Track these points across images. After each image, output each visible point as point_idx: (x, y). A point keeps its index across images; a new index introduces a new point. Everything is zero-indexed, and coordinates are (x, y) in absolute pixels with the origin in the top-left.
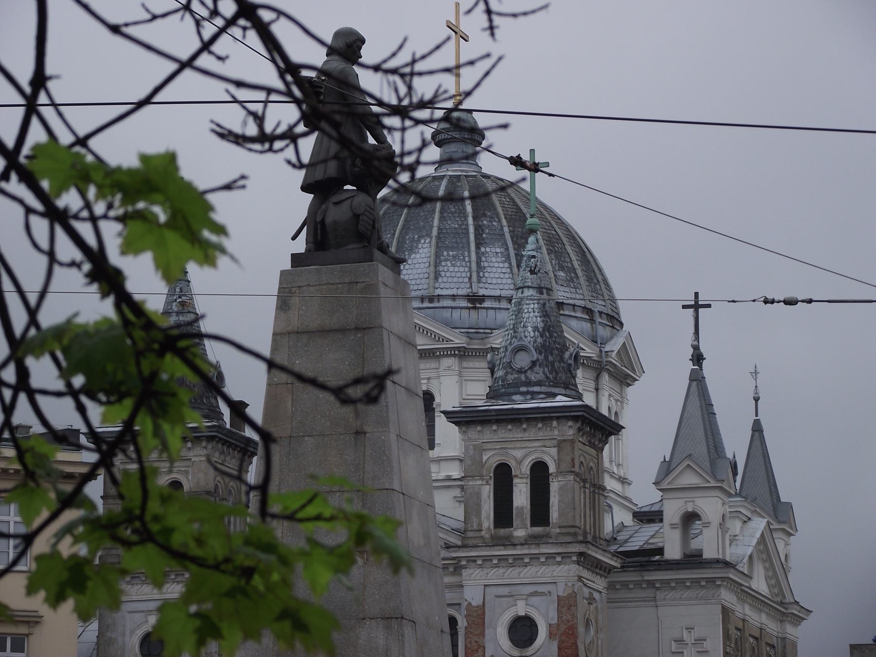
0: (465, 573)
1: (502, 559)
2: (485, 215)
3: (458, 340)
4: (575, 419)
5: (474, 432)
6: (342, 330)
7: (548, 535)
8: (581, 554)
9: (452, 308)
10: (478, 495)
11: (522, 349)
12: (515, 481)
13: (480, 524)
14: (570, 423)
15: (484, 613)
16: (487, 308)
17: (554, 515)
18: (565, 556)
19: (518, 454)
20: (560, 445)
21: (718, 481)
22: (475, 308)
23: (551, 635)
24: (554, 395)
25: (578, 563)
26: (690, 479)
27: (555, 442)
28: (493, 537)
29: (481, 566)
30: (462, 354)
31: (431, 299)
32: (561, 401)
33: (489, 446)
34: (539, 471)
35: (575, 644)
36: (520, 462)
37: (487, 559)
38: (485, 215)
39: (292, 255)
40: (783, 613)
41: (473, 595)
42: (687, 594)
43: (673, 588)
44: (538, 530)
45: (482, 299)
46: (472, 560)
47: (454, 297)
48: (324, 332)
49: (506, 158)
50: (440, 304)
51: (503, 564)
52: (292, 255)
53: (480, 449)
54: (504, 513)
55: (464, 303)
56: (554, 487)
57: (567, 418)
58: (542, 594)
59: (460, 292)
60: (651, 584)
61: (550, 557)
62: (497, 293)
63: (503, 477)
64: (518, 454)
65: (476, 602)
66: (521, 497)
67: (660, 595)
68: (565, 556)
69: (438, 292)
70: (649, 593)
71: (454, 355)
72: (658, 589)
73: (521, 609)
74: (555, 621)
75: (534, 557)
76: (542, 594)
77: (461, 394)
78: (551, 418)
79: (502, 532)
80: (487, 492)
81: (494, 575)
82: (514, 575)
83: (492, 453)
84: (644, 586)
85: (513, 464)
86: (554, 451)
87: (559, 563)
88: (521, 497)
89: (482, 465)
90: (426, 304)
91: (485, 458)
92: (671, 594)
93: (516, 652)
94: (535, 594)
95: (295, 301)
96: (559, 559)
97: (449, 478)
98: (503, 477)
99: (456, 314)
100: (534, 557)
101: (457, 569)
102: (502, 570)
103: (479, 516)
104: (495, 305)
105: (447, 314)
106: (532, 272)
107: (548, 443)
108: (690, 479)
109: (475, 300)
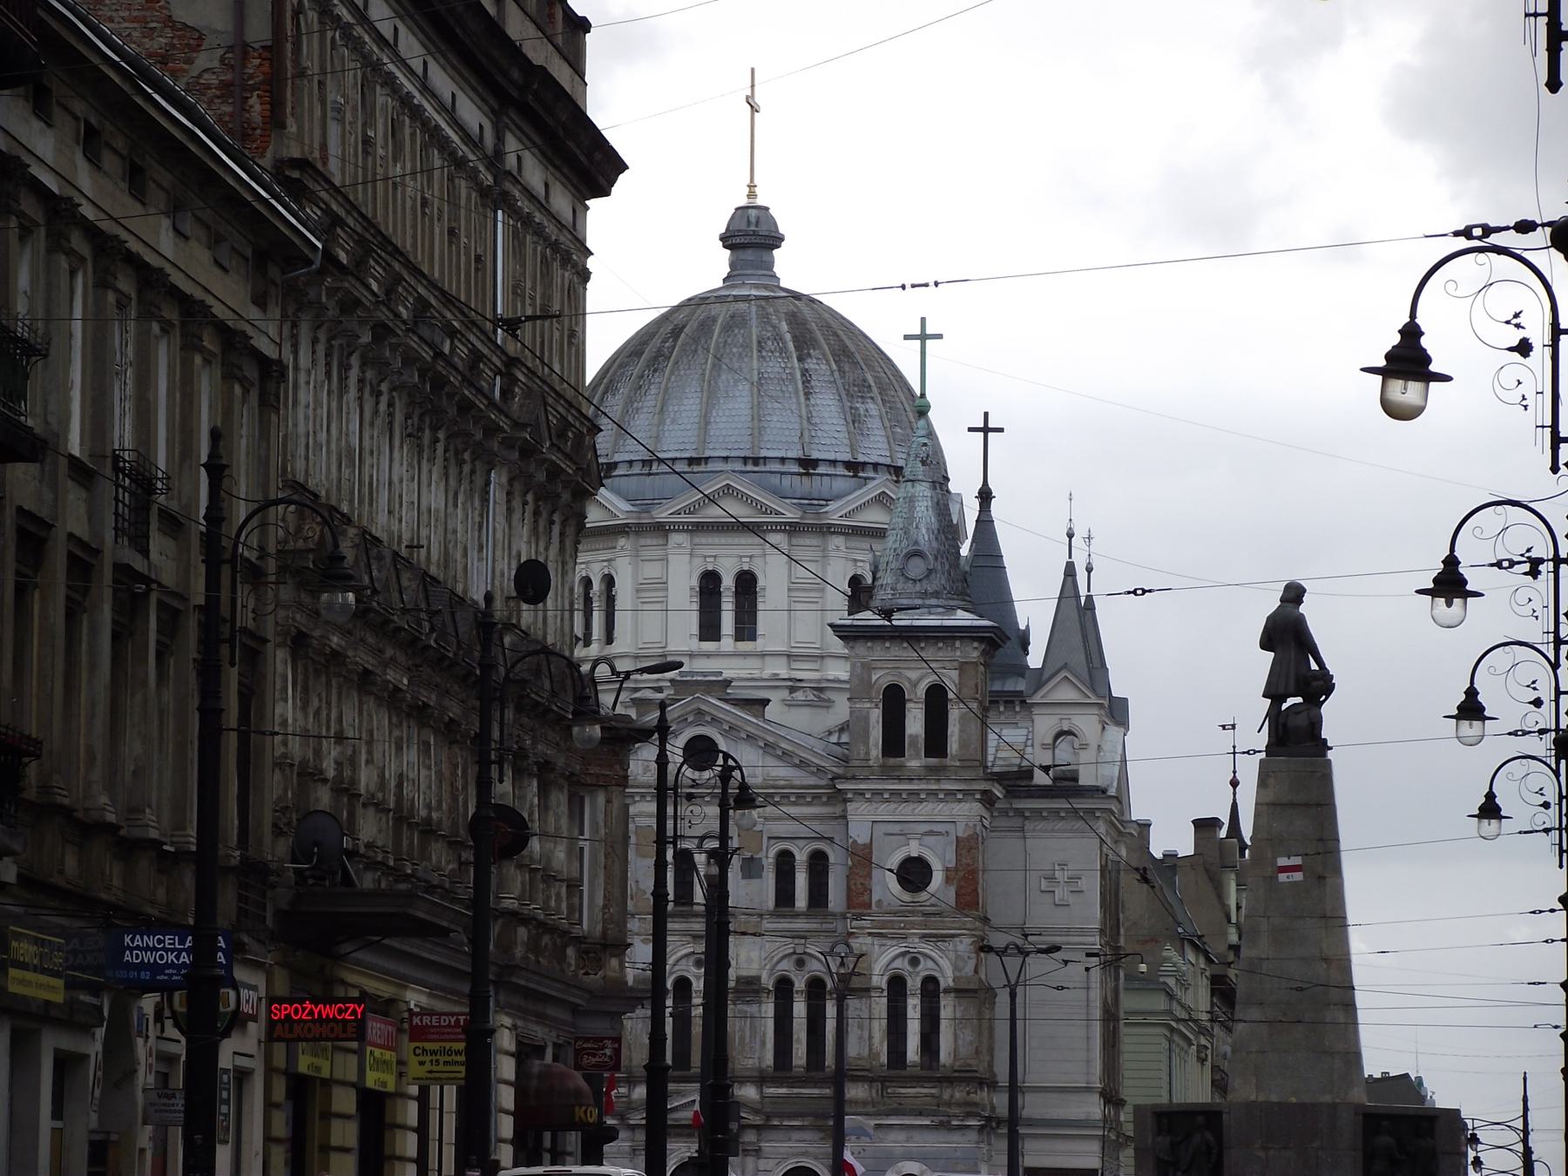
0: (850, 807)
1: (896, 793)
2: (809, 355)
3: (791, 515)
4: (981, 640)
5: (861, 649)
6: (1307, 805)
7: (945, 768)
8: (984, 792)
9: (782, 473)
10: (866, 719)
11: (917, 554)
12: (908, 705)
13: (868, 753)
14: (976, 644)
15: (871, 853)
16: (821, 475)
17: (953, 745)
18: (968, 793)
19: (913, 675)
20: (962, 667)
21: (1098, 696)
22: (807, 474)
23: (948, 880)
24: (952, 609)
25: (980, 801)
26: (1066, 694)
27: (956, 664)
28: (883, 766)
29: (869, 800)
30: (793, 529)
31: (756, 461)
32: (963, 618)
33: (879, 664)
34: (936, 699)
35: (976, 890)
36: (915, 685)
37: (877, 793)
38: (809, 355)
39: (620, 166)
40: (1120, 832)
41: (859, 832)
42: (1060, 825)
43: (1045, 818)
44: (932, 761)
45: (815, 463)
46: (861, 793)
47: (783, 460)
48: (1292, 805)
49: (752, 195)
50: (768, 468)
51: (894, 798)
52: (620, 166)
53: (868, 668)
54: (894, 741)
55: (795, 468)
56: (954, 714)
57: (973, 639)
58: (939, 834)
59: (790, 455)
60: (1020, 813)
61: (950, 793)
62: (831, 457)
63: (894, 700)
64: (913, 675)
65: (862, 839)
66: (915, 723)
67: (1029, 825)
68: (965, 792)
69: (764, 453)
70: (1017, 822)
71: (784, 531)
72: (1026, 818)
73: (914, 849)
74: (953, 864)
75: (932, 794)
76: (939, 834)
77: (790, 576)
78: (955, 638)
79: (892, 761)
80: (876, 715)
81: (884, 811)
82: (906, 811)
83: (882, 673)
84: (941, 796)
85: (906, 686)
86: (955, 674)
87: (960, 801)
88: (915, 723)
89: (870, 686)
90: (750, 467)
91: (874, 678)
92: (1041, 825)
93: (907, 897)
94: (931, 833)
95: (1271, 781)
96: (960, 796)
97: (775, 677)
98: (894, 700)
99: (786, 481)
100: (932, 794)
101: (838, 797)
102: (893, 806)
103: (866, 743)
104: (831, 471)
105: (775, 480)
106: (924, 463)
107: (948, 665)
108: (1066, 694)
109: (808, 464)
